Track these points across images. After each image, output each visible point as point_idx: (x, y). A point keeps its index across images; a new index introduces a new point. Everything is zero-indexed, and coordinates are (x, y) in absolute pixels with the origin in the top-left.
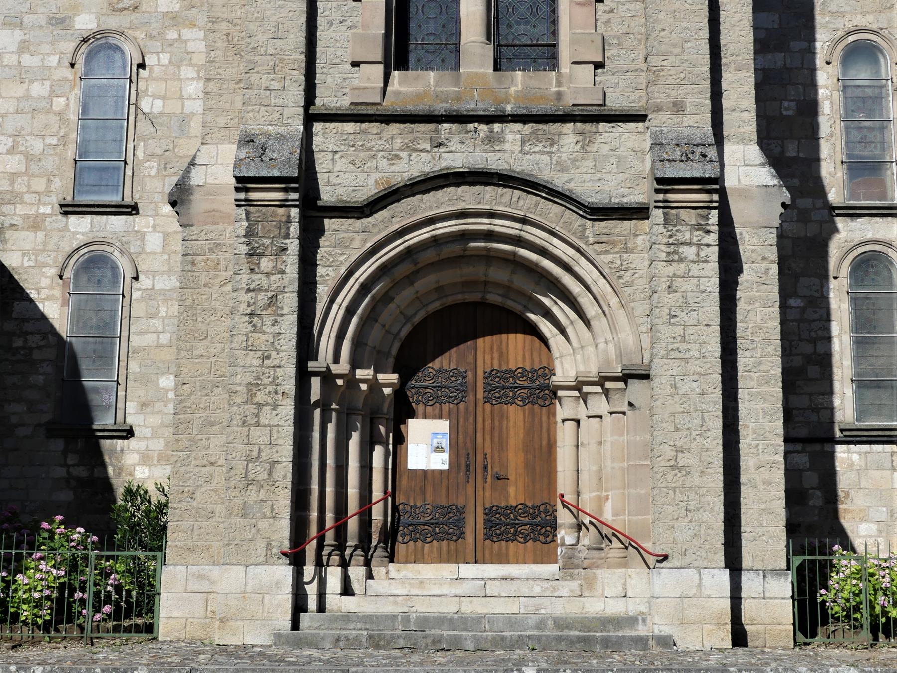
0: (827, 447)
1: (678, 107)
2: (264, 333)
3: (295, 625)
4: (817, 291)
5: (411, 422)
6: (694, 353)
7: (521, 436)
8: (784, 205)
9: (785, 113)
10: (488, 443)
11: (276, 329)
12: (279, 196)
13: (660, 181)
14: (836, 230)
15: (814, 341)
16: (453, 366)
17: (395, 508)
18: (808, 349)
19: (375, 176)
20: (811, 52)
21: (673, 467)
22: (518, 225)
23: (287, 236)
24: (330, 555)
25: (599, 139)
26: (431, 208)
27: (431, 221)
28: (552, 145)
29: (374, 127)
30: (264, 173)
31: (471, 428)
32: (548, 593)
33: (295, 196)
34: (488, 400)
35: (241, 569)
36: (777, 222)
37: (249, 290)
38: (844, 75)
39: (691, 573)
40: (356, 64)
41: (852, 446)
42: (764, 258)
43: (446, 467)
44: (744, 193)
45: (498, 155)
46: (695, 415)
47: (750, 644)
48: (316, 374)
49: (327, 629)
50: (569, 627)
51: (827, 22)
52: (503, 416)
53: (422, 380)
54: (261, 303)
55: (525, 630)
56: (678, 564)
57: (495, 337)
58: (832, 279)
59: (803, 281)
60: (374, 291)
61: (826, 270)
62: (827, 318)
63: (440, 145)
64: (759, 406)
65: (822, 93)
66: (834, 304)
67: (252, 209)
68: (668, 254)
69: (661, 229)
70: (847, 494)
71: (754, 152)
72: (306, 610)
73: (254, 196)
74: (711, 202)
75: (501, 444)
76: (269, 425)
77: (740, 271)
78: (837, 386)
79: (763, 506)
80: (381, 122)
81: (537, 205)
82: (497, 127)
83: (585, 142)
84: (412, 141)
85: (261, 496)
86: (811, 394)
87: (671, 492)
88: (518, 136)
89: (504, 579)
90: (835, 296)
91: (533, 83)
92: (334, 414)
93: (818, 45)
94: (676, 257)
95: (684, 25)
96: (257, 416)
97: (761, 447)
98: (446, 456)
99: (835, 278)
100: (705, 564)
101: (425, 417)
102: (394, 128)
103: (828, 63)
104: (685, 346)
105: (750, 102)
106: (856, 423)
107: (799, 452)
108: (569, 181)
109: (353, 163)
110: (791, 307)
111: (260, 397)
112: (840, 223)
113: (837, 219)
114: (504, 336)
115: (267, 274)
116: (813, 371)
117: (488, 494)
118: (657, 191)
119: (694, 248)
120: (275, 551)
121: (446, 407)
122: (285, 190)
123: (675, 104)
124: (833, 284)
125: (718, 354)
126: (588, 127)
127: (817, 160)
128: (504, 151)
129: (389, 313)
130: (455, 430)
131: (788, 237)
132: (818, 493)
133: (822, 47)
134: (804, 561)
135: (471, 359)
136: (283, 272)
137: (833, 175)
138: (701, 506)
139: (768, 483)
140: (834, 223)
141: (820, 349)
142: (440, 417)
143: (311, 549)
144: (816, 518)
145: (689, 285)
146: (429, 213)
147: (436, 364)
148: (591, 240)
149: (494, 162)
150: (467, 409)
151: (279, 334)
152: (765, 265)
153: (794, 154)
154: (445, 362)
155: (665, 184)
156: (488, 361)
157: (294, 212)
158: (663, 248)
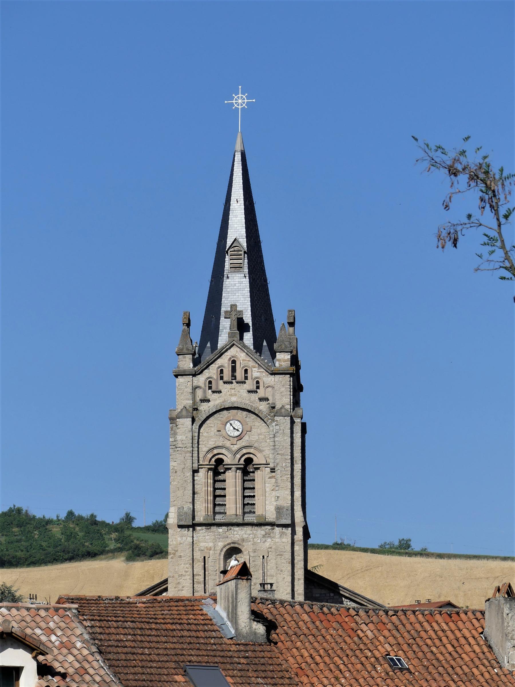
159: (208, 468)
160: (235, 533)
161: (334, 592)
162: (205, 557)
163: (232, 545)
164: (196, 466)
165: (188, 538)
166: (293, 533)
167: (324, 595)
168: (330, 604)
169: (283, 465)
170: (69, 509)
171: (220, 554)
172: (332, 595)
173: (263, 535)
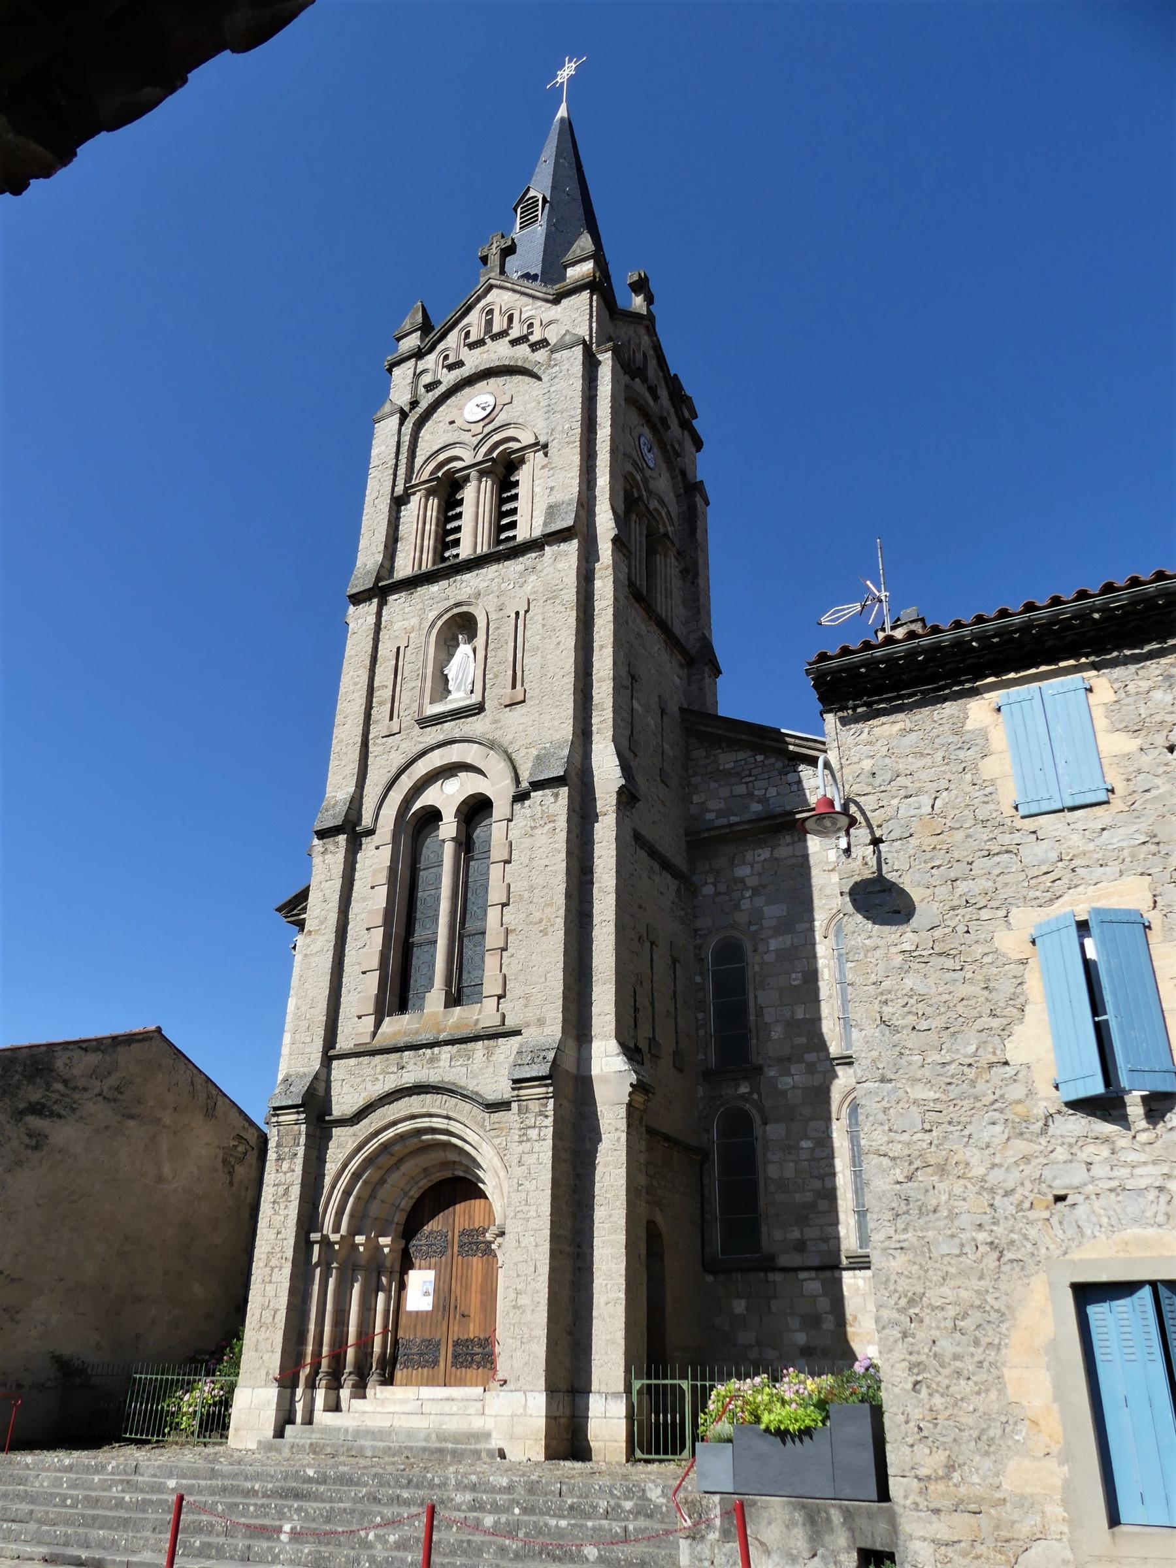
0: (836, 1274)
1: (541, 1022)
2: (279, 1215)
3: (279, 1433)
4: (823, 1132)
5: (411, 1272)
6: (533, 1214)
7: (480, 1280)
8: (632, 1085)
9: (793, 983)
10: (459, 1288)
11: (286, 1212)
12: (294, 1117)
13: (515, 1081)
14: (836, 1076)
15: (821, 1178)
16: (440, 1228)
17: (396, 1342)
18: (817, 1185)
19: (363, 1095)
20: (812, 930)
21: (514, 1307)
22: (446, 1121)
23: (298, 1145)
24: (321, 1380)
25: (498, 1051)
26: (394, 1114)
27: (394, 1123)
28: (468, 1059)
29: (365, 1060)
30: (284, 1104)
31: (448, 1276)
32: (461, 1412)
33: (303, 1116)
34: (459, 1252)
35: (250, 1390)
36: (626, 1099)
37: (274, 1185)
38: (838, 945)
39: (520, 1395)
40: (360, 1017)
41: (857, 1272)
42: (617, 1129)
43: (430, 1308)
44: (605, 1079)
45: (436, 1070)
46: (530, 1263)
47: (594, 1458)
48: (316, 1242)
49: (301, 1438)
50: (445, 1440)
51: (824, 904)
52: (469, 1266)
53: (419, 1242)
54: (279, 1194)
55: (417, 1441)
56: (513, 1388)
57: (468, 1203)
58: (834, 1121)
59: (813, 1124)
60: (364, 1177)
61: (829, 1112)
62: (831, 1157)
63: (402, 1068)
64: (608, 1251)
65: (821, 963)
66: (837, 1143)
67: (281, 1128)
68: (520, 1136)
69: (517, 1118)
70: (855, 1318)
71: (613, 1045)
72: (291, 1421)
73: (281, 1118)
74: (547, 1093)
75: (467, 1287)
76: (277, 1283)
77: (600, 1140)
78: (842, 1216)
79: (609, 1337)
80: (370, 1055)
81: (456, 1105)
82: (436, 1050)
83: (489, 1054)
84: (386, 1067)
85: (267, 1336)
86: (821, 1226)
87: (512, 1328)
88: (449, 1055)
89: (447, 1399)
90: (838, 1135)
91: (465, 1015)
92: (334, 1271)
93: (817, 923)
94: (525, 1138)
95: (547, 960)
96: (271, 1275)
97: (609, 1286)
98: (430, 1299)
99: (838, 1119)
100: (531, 1387)
101: (420, 1269)
102: (378, 1058)
103: (826, 937)
104: (527, 1208)
105: (610, 1008)
106: (859, 1250)
107: (812, 1279)
108: (477, 1085)
109: (352, 1086)
110: (803, 1149)
111: (273, 1262)
112: (840, 1070)
113: (837, 1068)
114: (473, 1201)
115: (285, 1173)
116: (822, 1205)
117: (456, 1328)
118: (513, 1089)
119: (537, 1130)
120: (271, 1377)
121: (433, 1260)
122: (298, 1113)
123: (539, 1020)
124: (835, 1125)
125: (548, 1213)
126: (491, 1043)
127: (820, 1019)
128: (440, 1067)
129: (384, 1192)
130: (438, 1278)
131: (799, 1088)
132: (830, 1317)
133: (821, 925)
134: (643, 1385)
135: (451, 1221)
136: (293, 1171)
137: (833, 1031)
138: (531, 1338)
139: (612, 1316)
140: (834, 1071)
141: (828, 1185)
142: (430, 1269)
143: (304, 1373)
144: (829, 1342)
145: (530, 1160)
146: (392, 1118)
147: (427, 1228)
148: (488, 1128)
149: (431, 1076)
150: (446, 1260)
151: (287, 1215)
152: (618, 1134)
153: (802, 1017)
154: (432, 1226)
155: (518, 1082)
156: (462, 1223)
157: (303, 1127)
158: (517, 1132)
159: (424, 489)
160: (464, 584)
161: (763, 750)
162: (398, 648)
163: (456, 611)
164: (399, 490)
165: (368, 618)
166: (588, 557)
167: (743, 762)
168: (1147, 1254)
169: (566, 427)
170: (1068, 1284)
171: (429, 632)
172: (760, 758)
173: (521, 573)
